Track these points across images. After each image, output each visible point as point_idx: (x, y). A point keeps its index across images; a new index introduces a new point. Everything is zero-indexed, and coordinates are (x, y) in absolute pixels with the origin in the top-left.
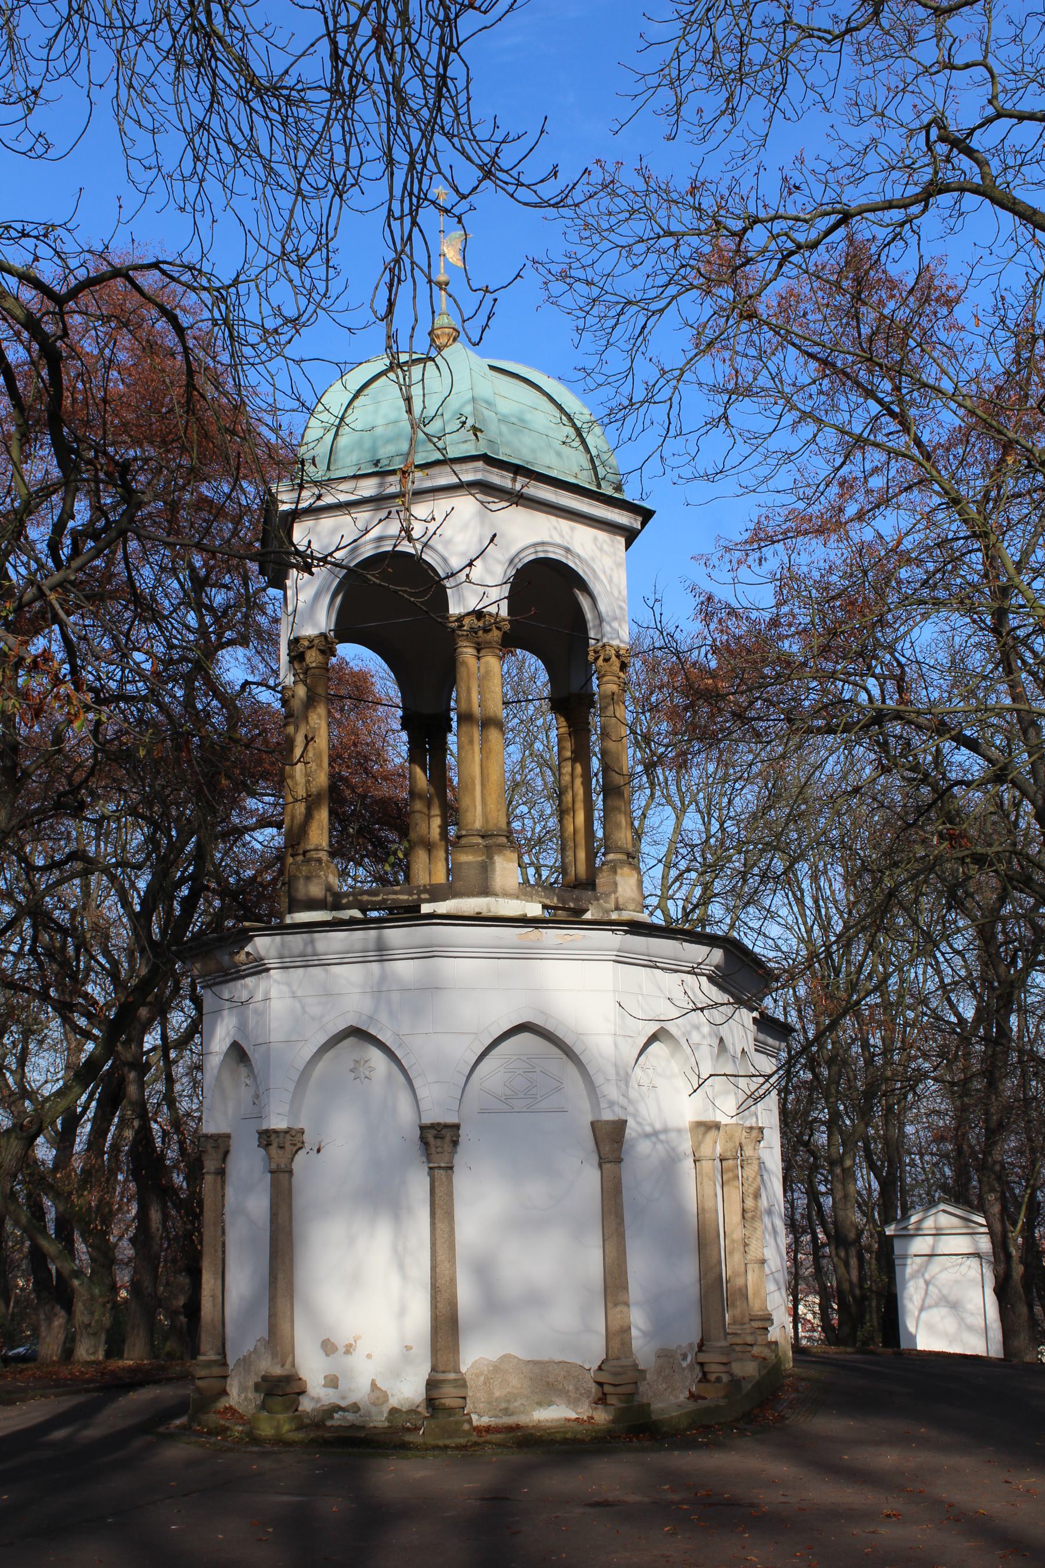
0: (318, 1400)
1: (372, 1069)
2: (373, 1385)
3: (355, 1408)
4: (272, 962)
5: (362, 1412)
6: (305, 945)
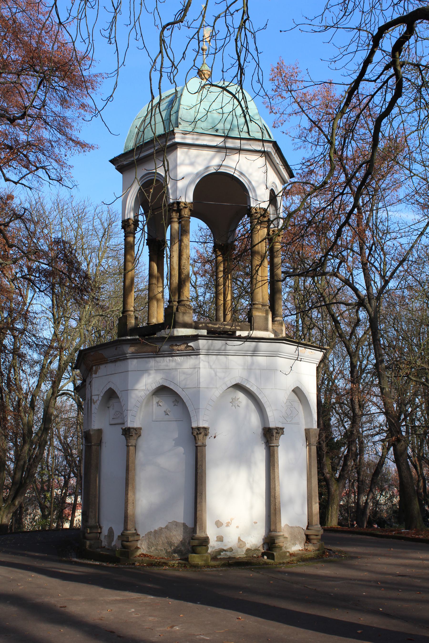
0: (214, 547)
1: (240, 402)
2: (239, 539)
3: (231, 550)
4: (202, 352)
5: (234, 551)
6: (222, 345)
